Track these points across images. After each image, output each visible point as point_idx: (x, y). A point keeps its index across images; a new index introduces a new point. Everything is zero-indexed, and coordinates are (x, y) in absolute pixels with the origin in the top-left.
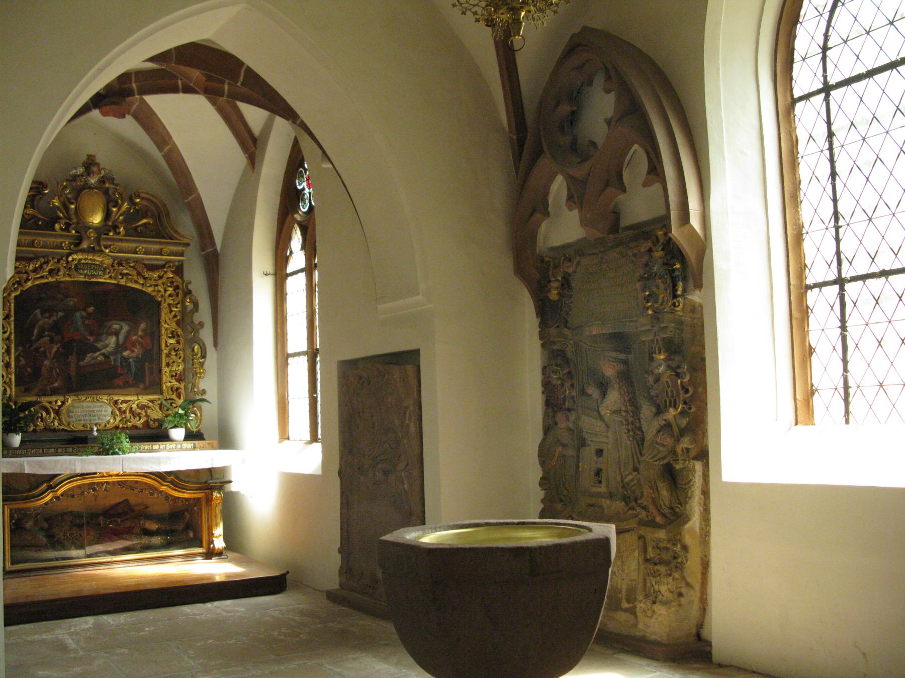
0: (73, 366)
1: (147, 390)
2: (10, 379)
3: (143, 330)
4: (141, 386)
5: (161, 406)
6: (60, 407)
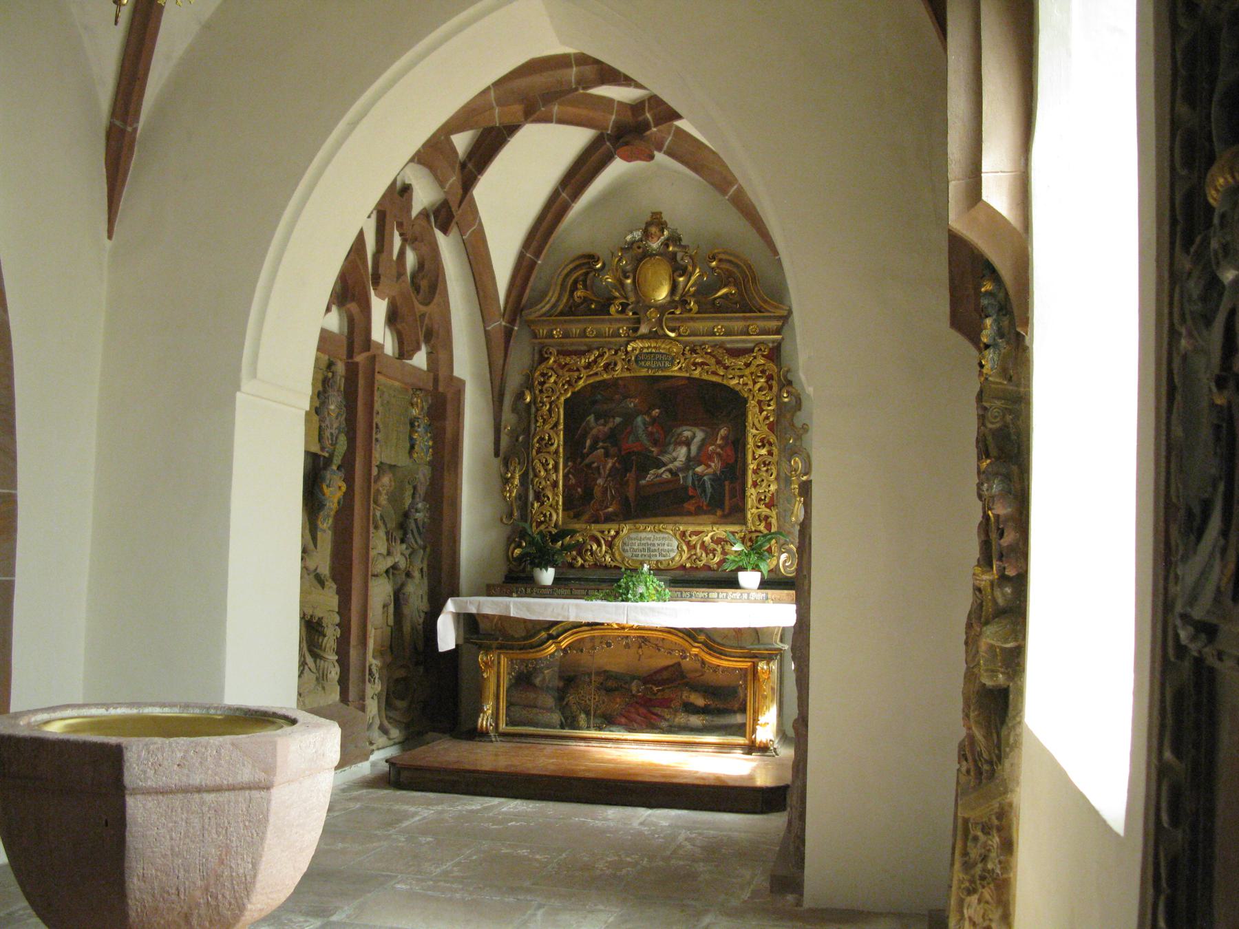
0: (632, 485)
2: (557, 502)
3: (722, 438)
4: (719, 513)
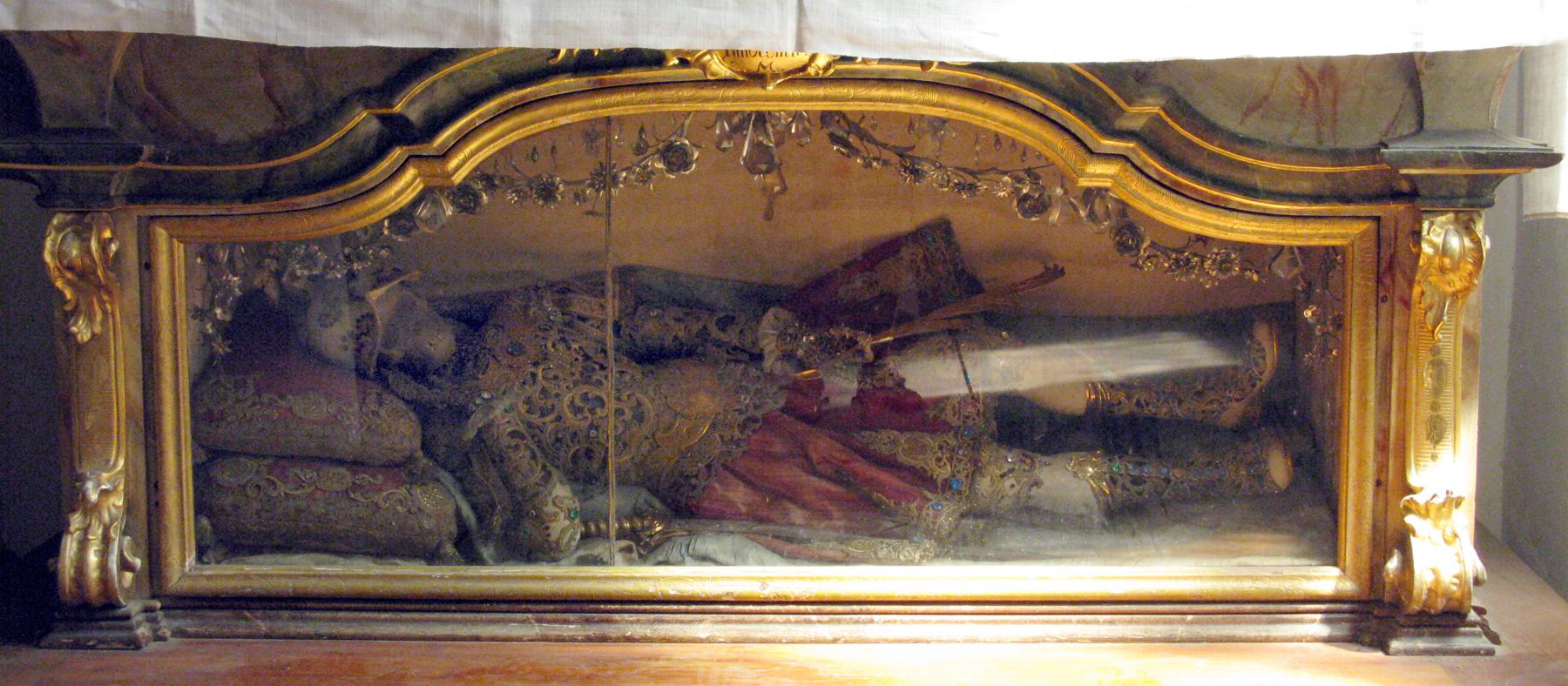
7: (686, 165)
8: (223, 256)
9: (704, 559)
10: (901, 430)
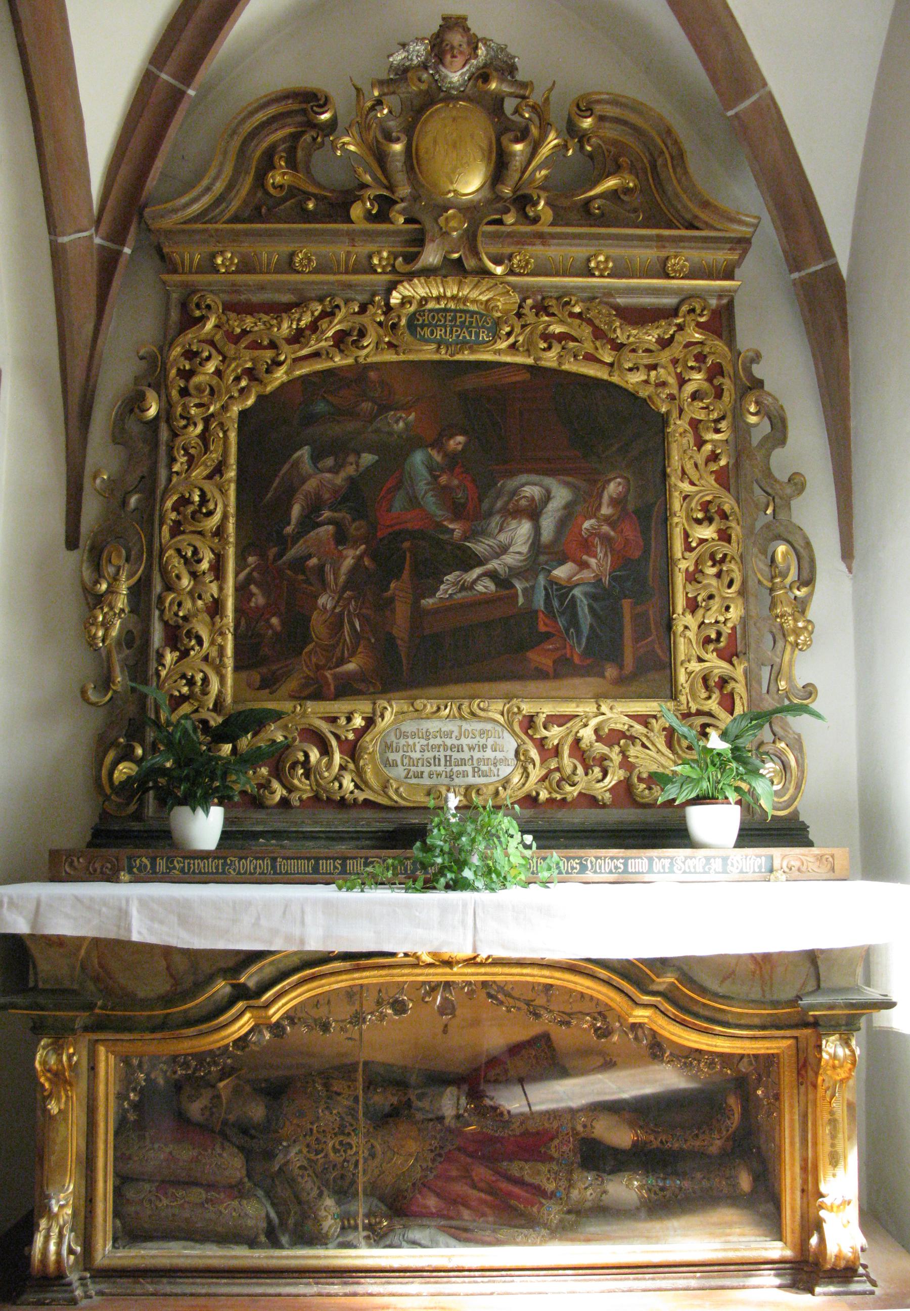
0: (402, 611)
1: (626, 686)
2: (221, 650)
3: (614, 502)
5: (670, 735)
6: (361, 733)
7: (404, 1011)
8: (135, 1062)
9: (415, 1244)
10: (526, 1161)
